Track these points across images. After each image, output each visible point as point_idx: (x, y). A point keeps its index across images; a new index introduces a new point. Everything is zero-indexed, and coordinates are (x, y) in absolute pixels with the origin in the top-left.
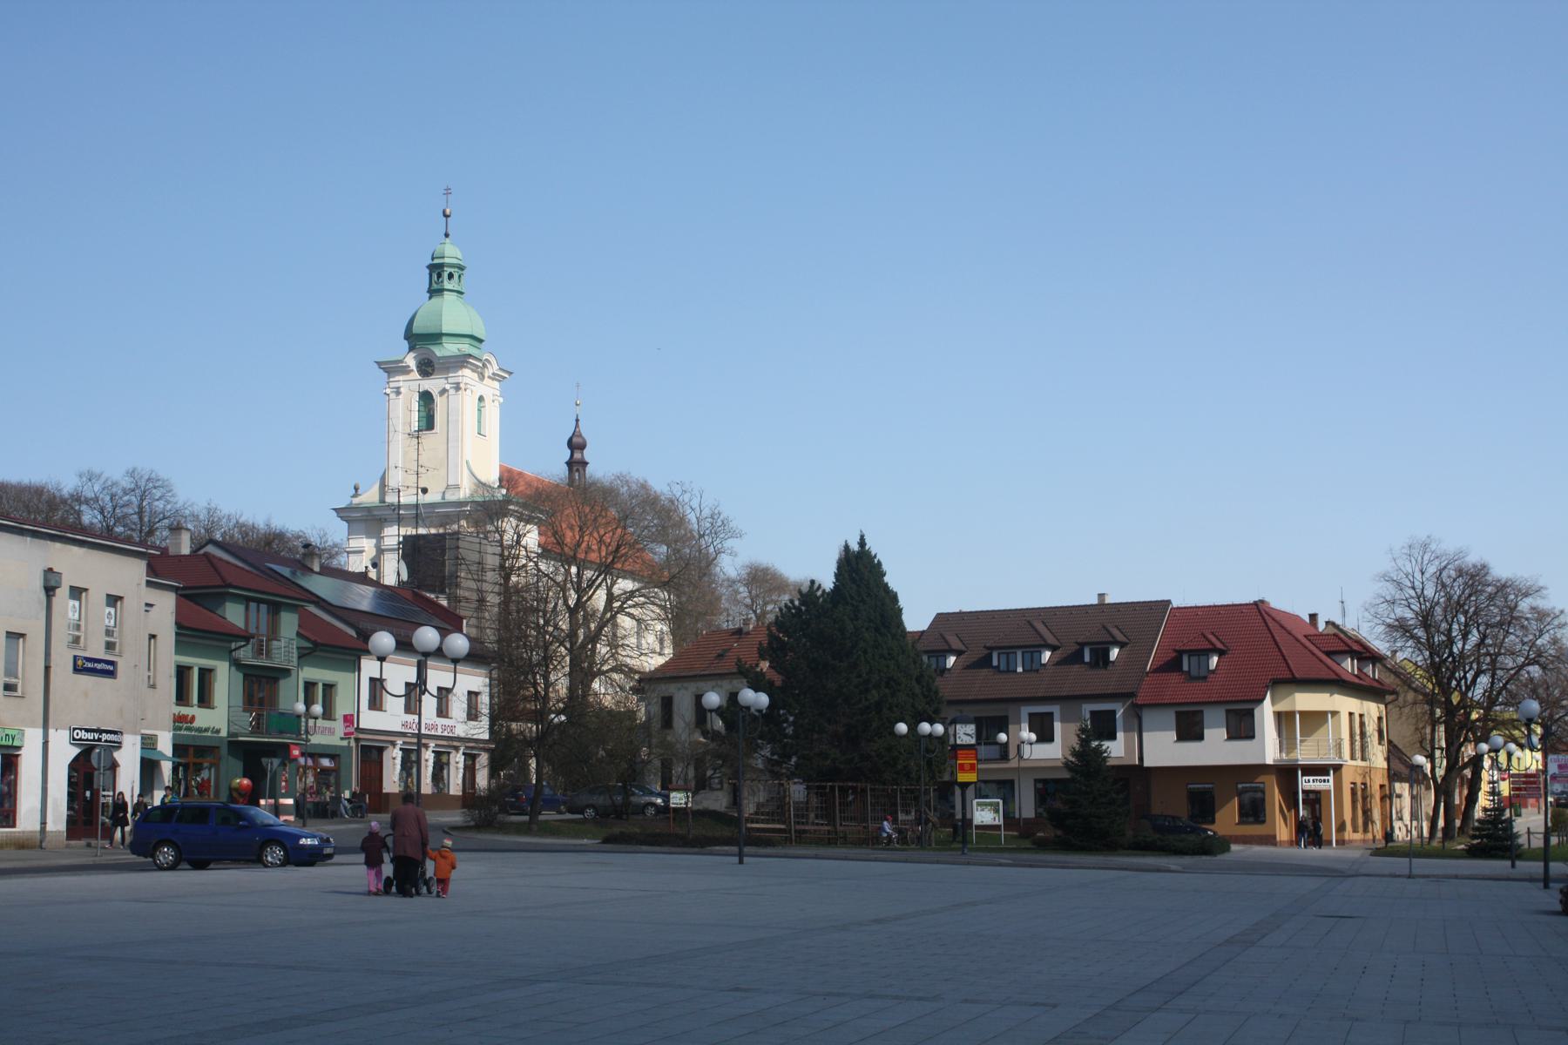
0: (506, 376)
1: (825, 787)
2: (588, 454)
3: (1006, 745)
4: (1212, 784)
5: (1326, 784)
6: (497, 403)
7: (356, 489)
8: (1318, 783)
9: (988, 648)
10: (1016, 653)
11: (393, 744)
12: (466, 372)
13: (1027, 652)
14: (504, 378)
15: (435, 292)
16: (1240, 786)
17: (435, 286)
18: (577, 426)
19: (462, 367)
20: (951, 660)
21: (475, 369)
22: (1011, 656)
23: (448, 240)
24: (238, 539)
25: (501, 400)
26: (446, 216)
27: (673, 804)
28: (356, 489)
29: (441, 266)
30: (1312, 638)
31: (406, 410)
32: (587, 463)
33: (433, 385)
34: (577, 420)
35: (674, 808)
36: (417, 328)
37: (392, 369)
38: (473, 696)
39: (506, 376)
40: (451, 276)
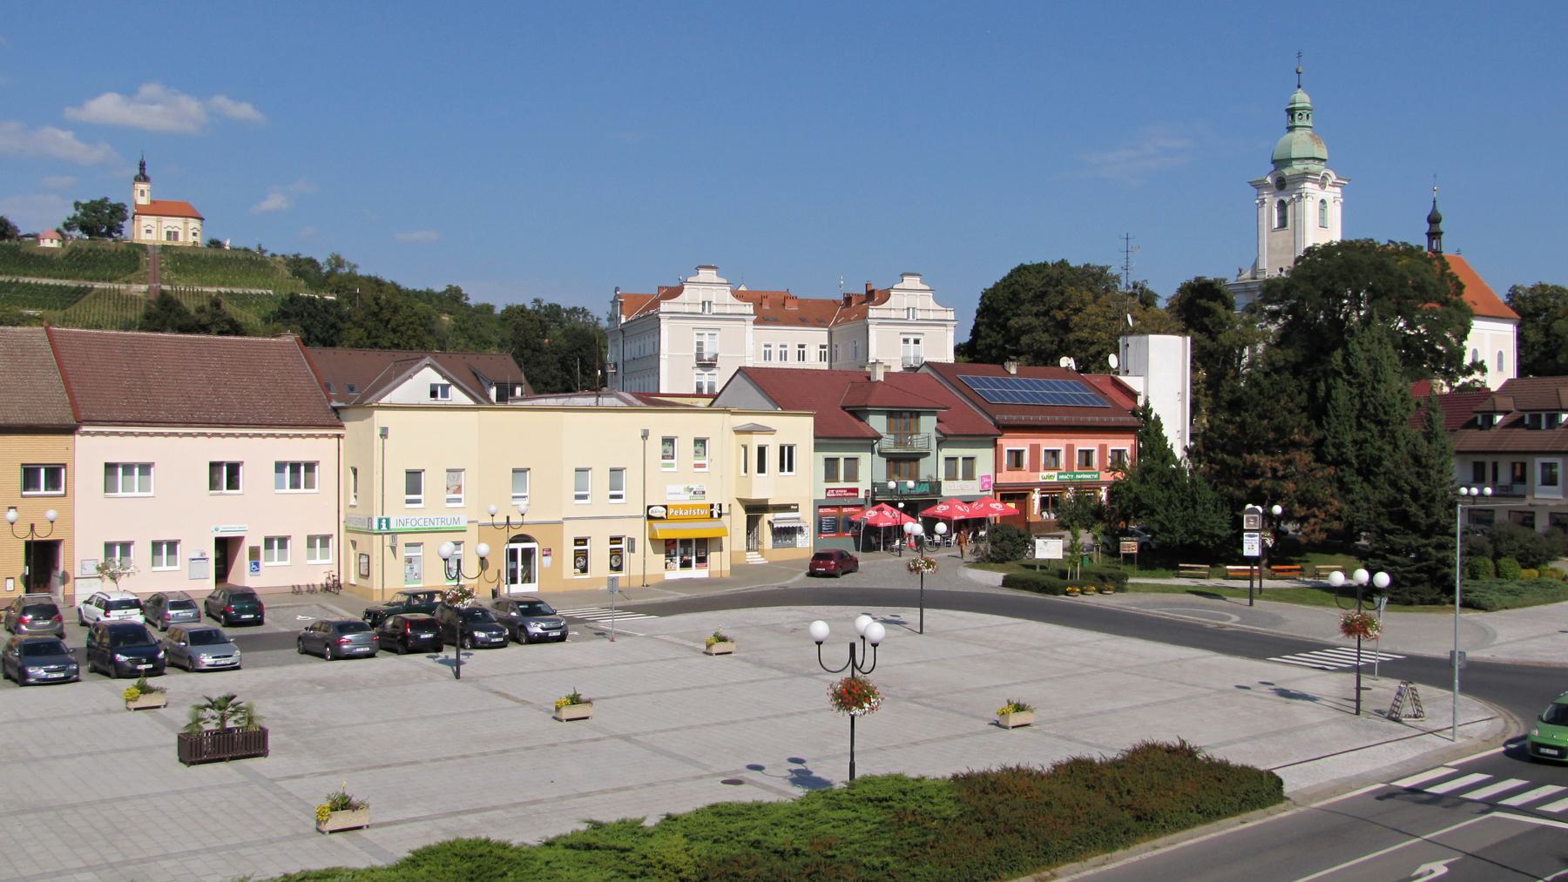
2: (1442, 226)
3: (1225, 551)
6: (1337, 203)
7: (1240, 271)
9: (1522, 411)
12: (1308, 185)
17: (1290, 124)
18: (1434, 206)
19: (1304, 182)
20: (1499, 418)
21: (1315, 181)
23: (1300, 90)
26: (1299, 73)
28: (1240, 271)
29: (1294, 109)
31: (1270, 214)
32: (1442, 233)
34: (1435, 202)
36: (1275, 158)
37: (1259, 186)
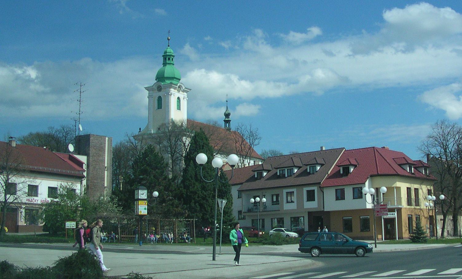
0: (189, 90)
1: (189, 221)
4: (352, 217)
5: (394, 215)
8: (390, 215)
10: (285, 170)
11: (21, 208)
13: (281, 170)
14: (188, 91)
15: (165, 64)
16: (361, 217)
22: (284, 171)
23: (169, 47)
24: (128, 147)
25: (187, 98)
26: (169, 40)
27: (67, 227)
30: (395, 159)
33: (161, 94)
35: (68, 229)
38: (416, 190)
39: (189, 90)
40: (169, 59)
